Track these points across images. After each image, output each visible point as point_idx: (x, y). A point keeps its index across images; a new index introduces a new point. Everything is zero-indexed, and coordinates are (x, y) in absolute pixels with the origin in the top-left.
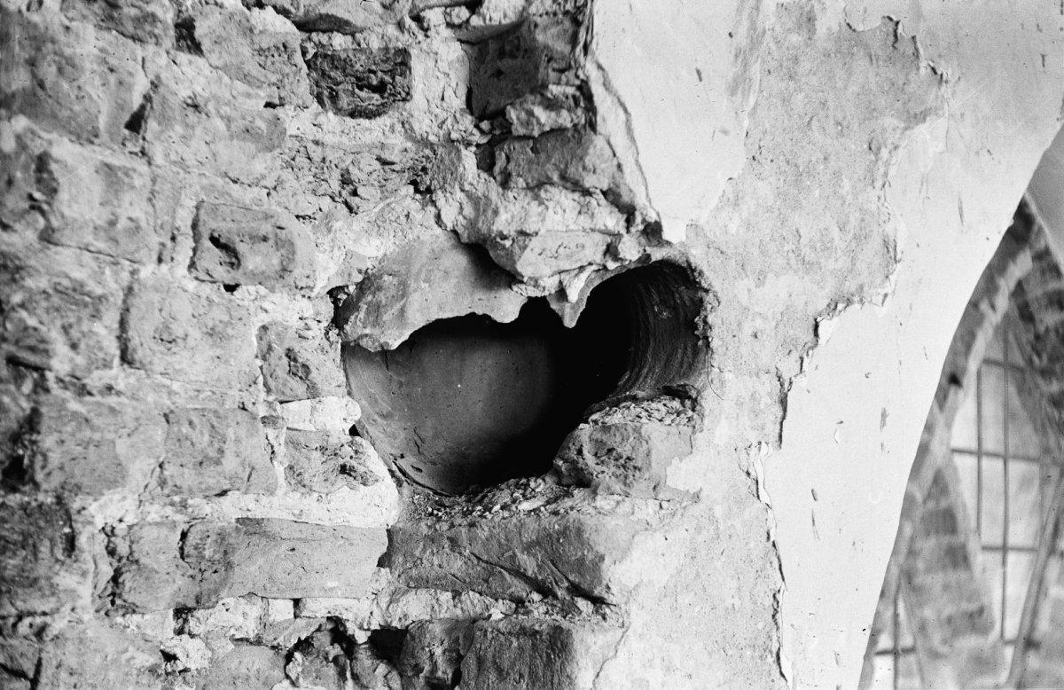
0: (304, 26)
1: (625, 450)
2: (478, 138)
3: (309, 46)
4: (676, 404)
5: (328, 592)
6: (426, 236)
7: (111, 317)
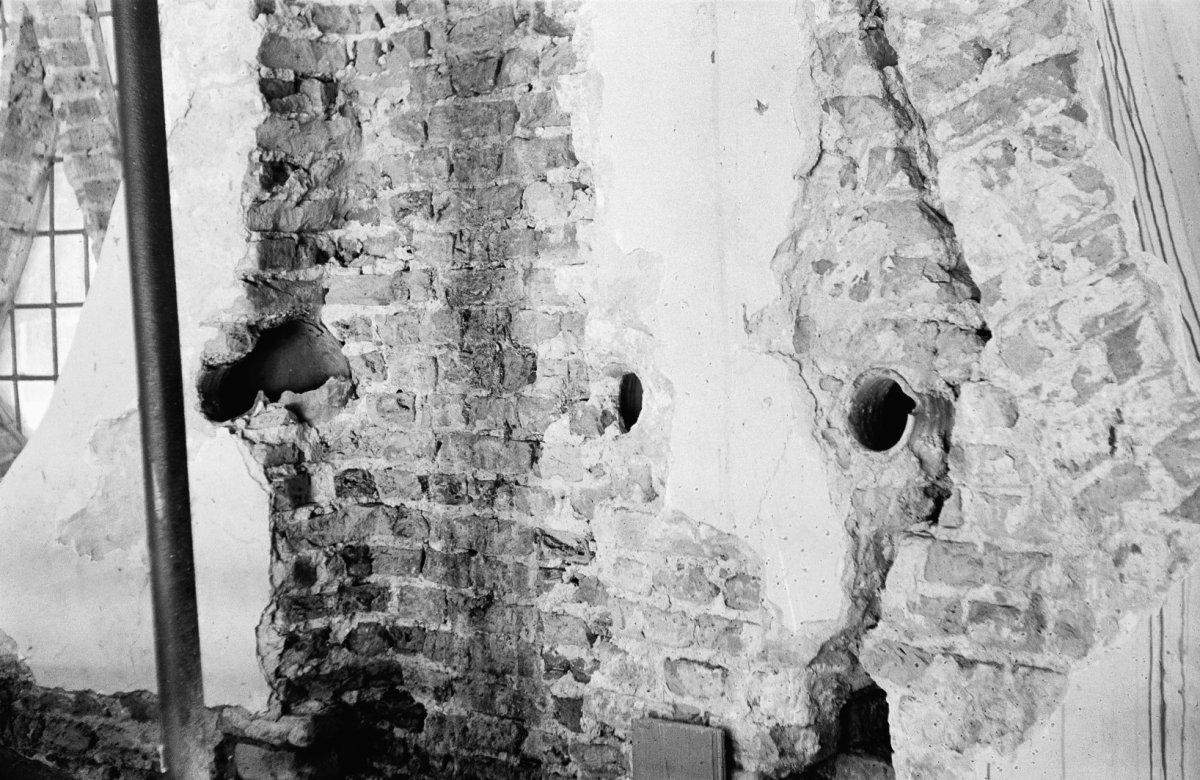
0: (378, 504)
1: (236, 341)
2: (306, 464)
3: (376, 497)
4: (211, 363)
5: (350, 278)
6: (322, 424)
7: (441, 373)
